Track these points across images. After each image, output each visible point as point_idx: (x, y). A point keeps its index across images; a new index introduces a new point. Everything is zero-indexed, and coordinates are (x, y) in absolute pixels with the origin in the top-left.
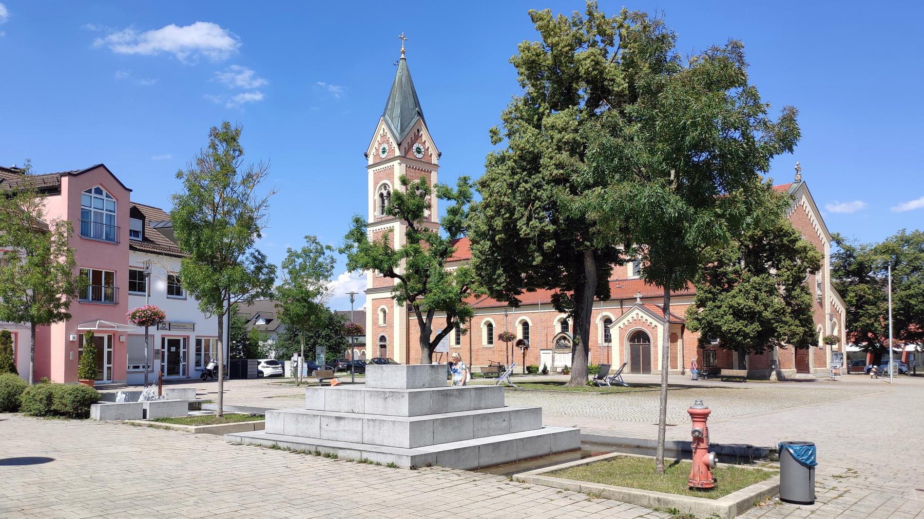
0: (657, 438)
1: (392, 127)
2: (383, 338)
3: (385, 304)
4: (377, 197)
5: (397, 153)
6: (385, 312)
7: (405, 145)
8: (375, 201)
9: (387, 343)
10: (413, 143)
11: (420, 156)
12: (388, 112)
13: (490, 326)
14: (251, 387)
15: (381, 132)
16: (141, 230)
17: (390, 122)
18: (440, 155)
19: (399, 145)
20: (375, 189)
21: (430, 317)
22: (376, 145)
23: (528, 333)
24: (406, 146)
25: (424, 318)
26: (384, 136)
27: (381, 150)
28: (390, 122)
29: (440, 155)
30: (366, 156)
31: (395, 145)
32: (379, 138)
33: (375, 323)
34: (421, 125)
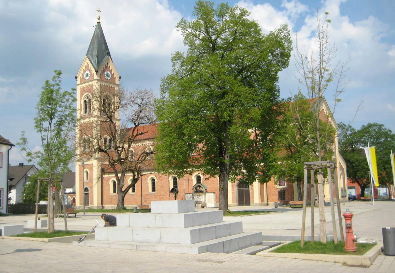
0: (301, 235)
1: (92, 61)
2: (86, 189)
3: (88, 168)
4: (82, 103)
5: (96, 77)
6: (87, 173)
7: (100, 72)
8: (81, 105)
9: (89, 192)
10: (104, 71)
11: (109, 78)
12: (90, 53)
13: (153, 180)
14: (370, 204)
15: (86, 64)
16: (47, 135)
17: (91, 58)
18: (120, 78)
19: (97, 72)
20: (81, 98)
21: (123, 175)
22: (82, 72)
23: (177, 184)
24: (101, 72)
25: (120, 175)
26: (87, 67)
27: (85, 75)
28: (91, 58)
29: (120, 78)
30: (76, 78)
31: (94, 72)
32: (84, 68)
33: (82, 179)
34: (109, 60)
